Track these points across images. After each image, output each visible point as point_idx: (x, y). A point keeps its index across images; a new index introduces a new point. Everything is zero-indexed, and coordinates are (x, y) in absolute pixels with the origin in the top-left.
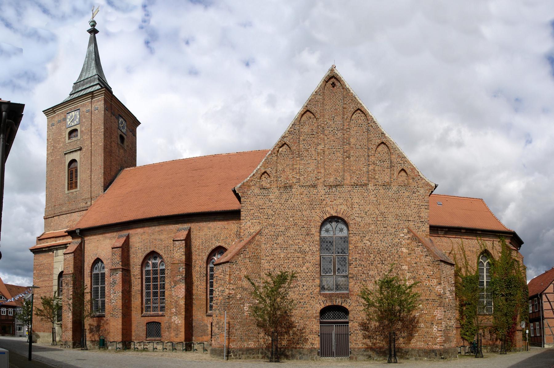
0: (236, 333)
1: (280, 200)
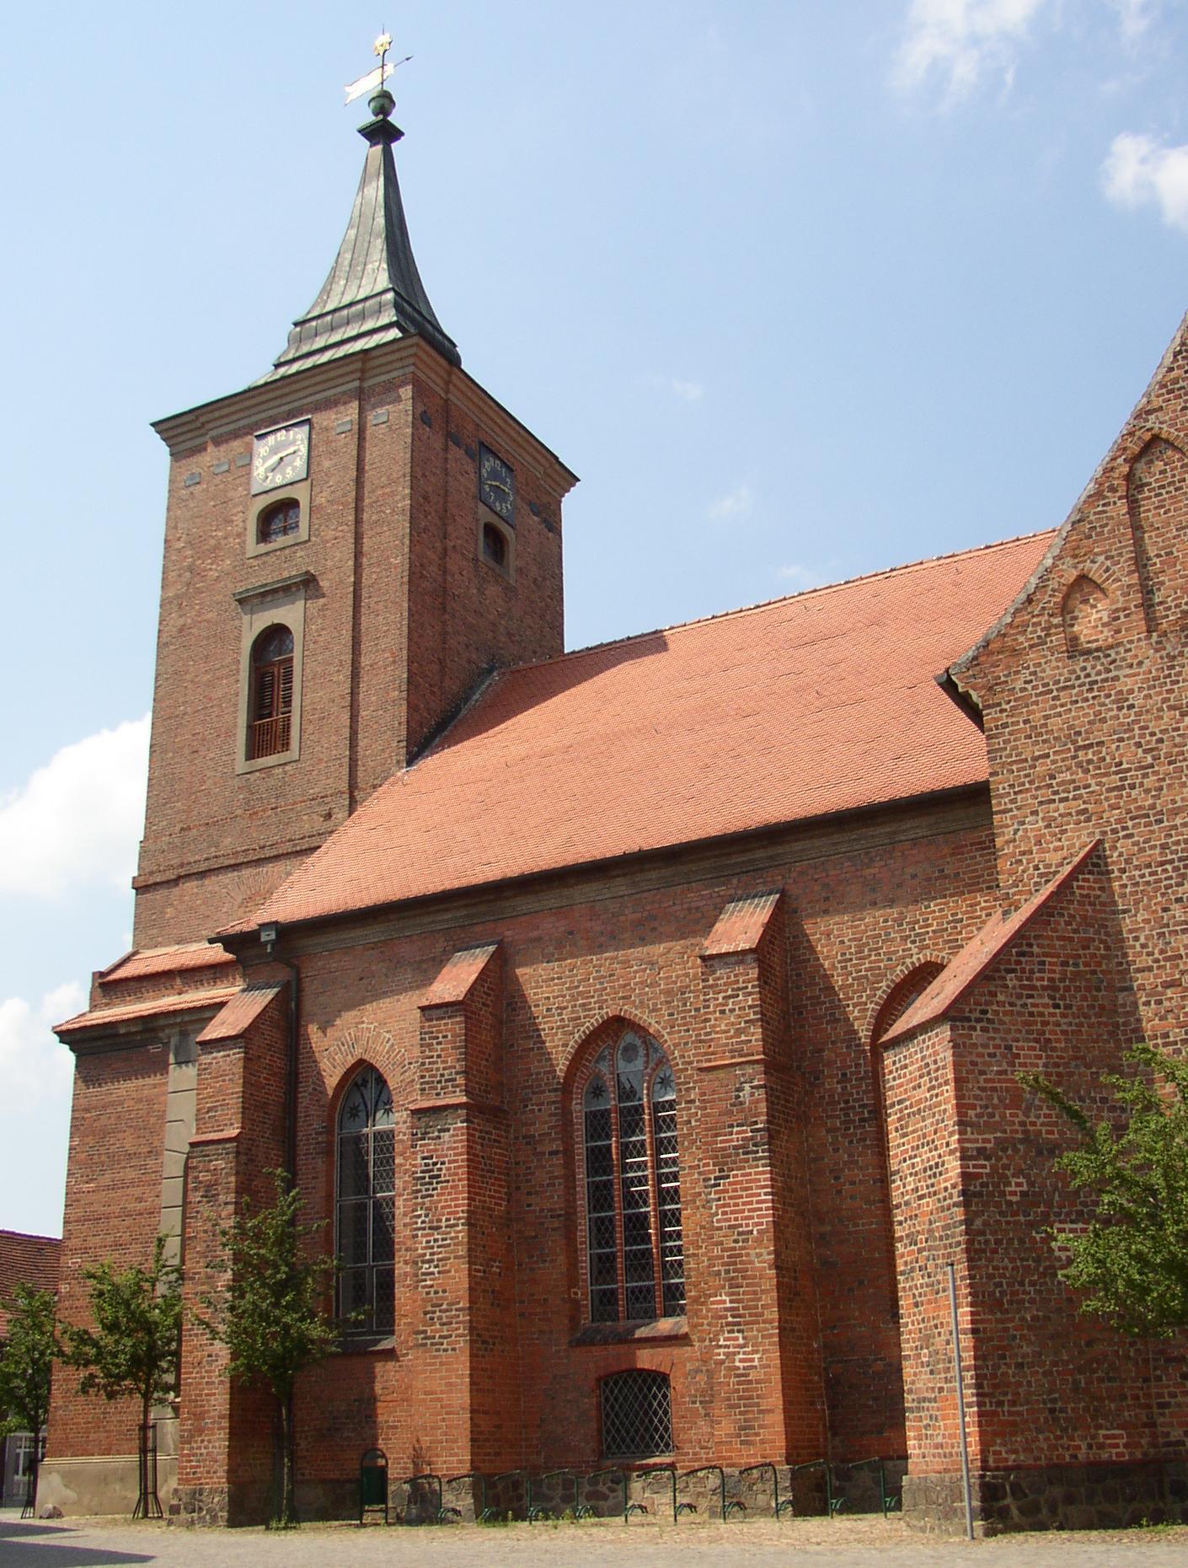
0: (1019, 1384)
1: (1170, 691)
